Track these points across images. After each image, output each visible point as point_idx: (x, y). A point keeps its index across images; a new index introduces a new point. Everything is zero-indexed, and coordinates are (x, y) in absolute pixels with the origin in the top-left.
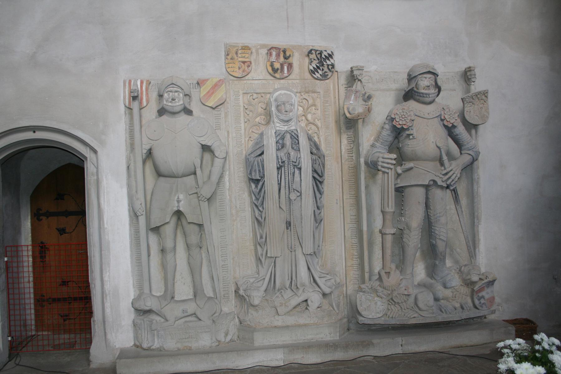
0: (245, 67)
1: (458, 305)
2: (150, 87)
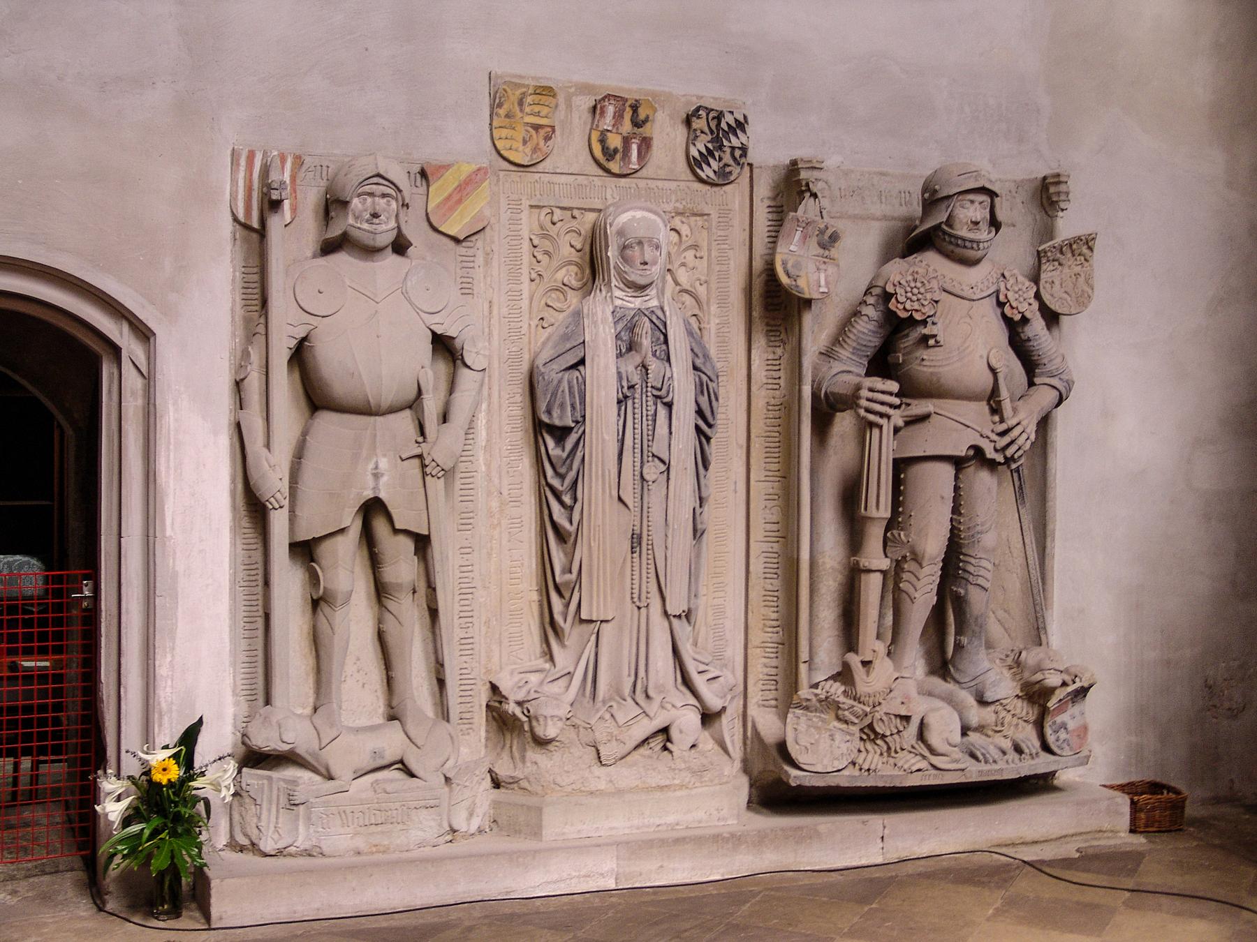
0: (538, 138)
1: (1007, 745)
2: (301, 175)
